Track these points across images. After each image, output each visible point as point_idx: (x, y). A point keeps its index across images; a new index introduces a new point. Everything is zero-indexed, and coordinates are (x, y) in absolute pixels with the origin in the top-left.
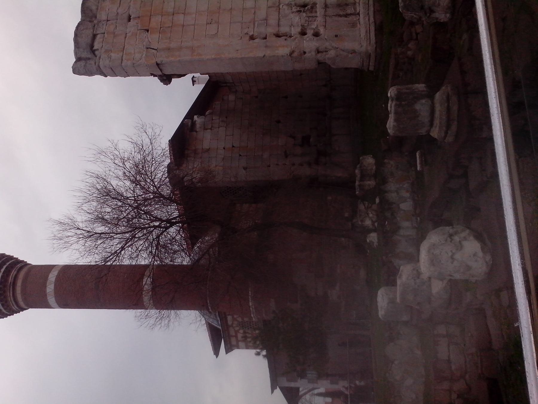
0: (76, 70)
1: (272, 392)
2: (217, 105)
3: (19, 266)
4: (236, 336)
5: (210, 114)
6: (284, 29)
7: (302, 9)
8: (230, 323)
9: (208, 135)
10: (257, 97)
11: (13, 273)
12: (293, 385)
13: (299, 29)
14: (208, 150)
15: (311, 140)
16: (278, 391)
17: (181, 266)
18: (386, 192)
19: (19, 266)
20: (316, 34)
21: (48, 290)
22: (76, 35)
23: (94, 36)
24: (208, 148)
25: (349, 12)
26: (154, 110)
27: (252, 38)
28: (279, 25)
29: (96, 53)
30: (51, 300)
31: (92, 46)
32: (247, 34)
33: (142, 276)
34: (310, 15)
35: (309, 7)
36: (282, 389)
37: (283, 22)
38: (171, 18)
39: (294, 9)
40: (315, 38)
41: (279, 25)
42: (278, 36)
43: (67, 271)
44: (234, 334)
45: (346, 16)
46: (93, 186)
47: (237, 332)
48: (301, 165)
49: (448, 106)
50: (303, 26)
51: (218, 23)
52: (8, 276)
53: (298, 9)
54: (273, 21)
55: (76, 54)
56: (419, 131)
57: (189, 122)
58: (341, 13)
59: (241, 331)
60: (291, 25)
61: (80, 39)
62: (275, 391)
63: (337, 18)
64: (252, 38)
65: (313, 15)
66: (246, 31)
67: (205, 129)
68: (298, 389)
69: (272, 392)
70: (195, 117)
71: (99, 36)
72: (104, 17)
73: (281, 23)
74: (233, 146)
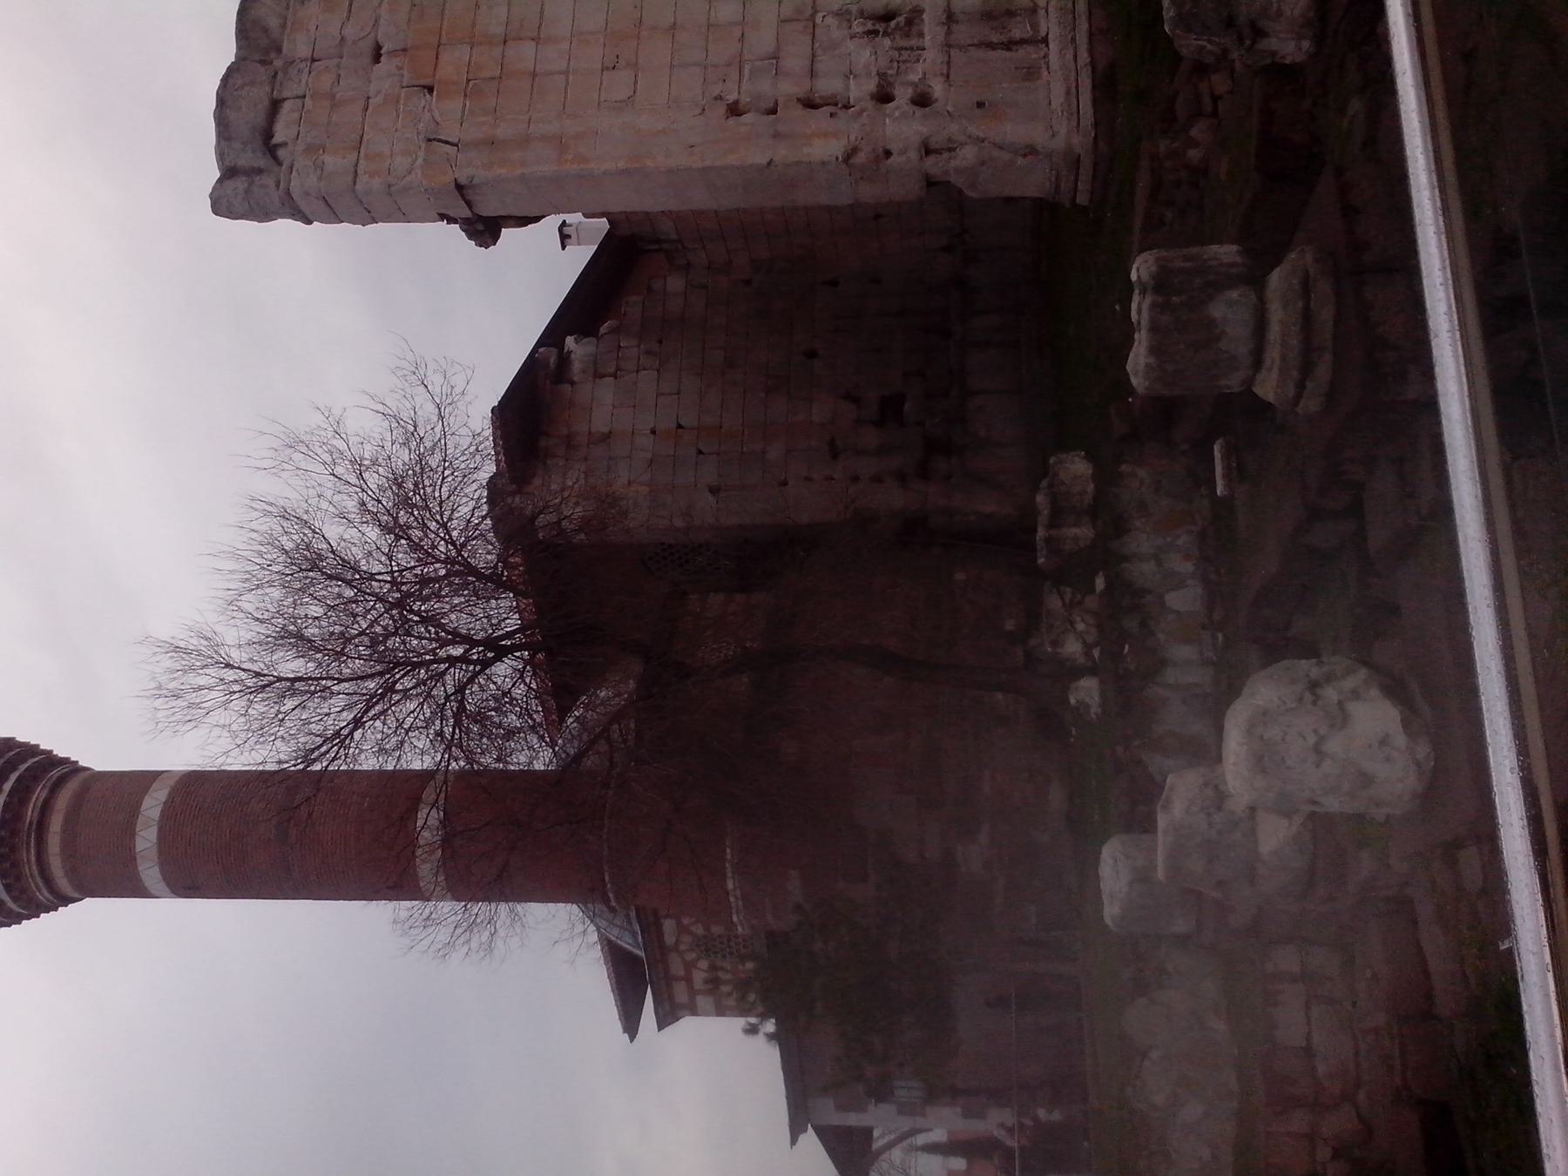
0: (222, 205)
1: (794, 1141)
2: (633, 306)
3: (55, 773)
4: (688, 979)
5: (613, 331)
6: (828, 85)
7: (880, 27)
8: (669, 939)
9: (606, 392)
10: (748, 282)
11: (39, 794)
12: (853, 1120)
13: (871, 85)
14: (606, 437)
15: (907, 407)
16: (810, 1139)
17: (528, 775)
19: (55, 773)
20: (922, 100)
21: (140, 845)
22: (222, 101)
23: (275, 106)
24: (606, 430)
25: (1017, 34)
26: (449, 319)
27: (734, 110)
28: (812, 74)
29: (281, 153)
30: (150, 873)
31: (268, 134)
32: (719, 98)
33: (415, 803)
34: (903, 43)
35: (901, 19)
36: (821, 1132)
37: (825, 63)
38: (497, 51)
39: (858, 28)
40: (919, 112)
41: (812, 74)
42: (810, 104)
43: (196, 790)
44: (682, 973)
45: (1009, 45)
46: (272, 542)
47: (690, 966)
48: (877, 479)
49: (1307, 308)
50: (882, 75)
51: (634, 66)
52: (23, 802)
53: (870, 25)
54: (795, 61)
55: (221, 156)
56: (1222, 383)
57: (552, 355)
58: (995, 39)
59: (703, 964)
60: (849, 74)
61: (232, 115)
62: (802, 1138)
63: (981, 53)
64: (734, 110)
65: (913, 42)
66: (716, 90)
67: (599, 375)
68: (867, 1133)
69: (794, 1141)
70: (570, 341)
71: (287, 105)
72: (303, 50)
73: (819, 67)
74: (680, 426)
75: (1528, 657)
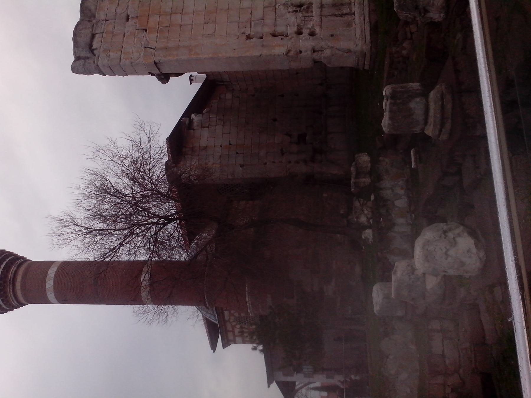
0: (75, 69)
1: (269, 386)
2: (214, 103)
3: (19, 262)
4: (233, 331)
5: (207, 112)
7: (298, 9)
8: (227, 318)
9: (205, 133)
11: (13, 269)
12: (289, 379)
17: (179, 262)
18: (381, 189)
19: (19, 262)
21: (48, 286)
25: (344, 11)
28: (275, 25)
30: (51, 295)
31: (91, 45)
33: (140, 272)
34: (306, 15)
43: (66, 267)
45: (342, 15)
46: (92, 184)
47: (234, 327)
53: (294, 9)
56: (414, 129)
57: (187, 120)
58: (337, 13)
59: (238, 326)
61: (79, 39)
63: (332, 18)
67: (203, 127)
68: (294, 383)
69: (269, 386)
70: (193, 115)
74: (230, 144)
75: (517, 223)
